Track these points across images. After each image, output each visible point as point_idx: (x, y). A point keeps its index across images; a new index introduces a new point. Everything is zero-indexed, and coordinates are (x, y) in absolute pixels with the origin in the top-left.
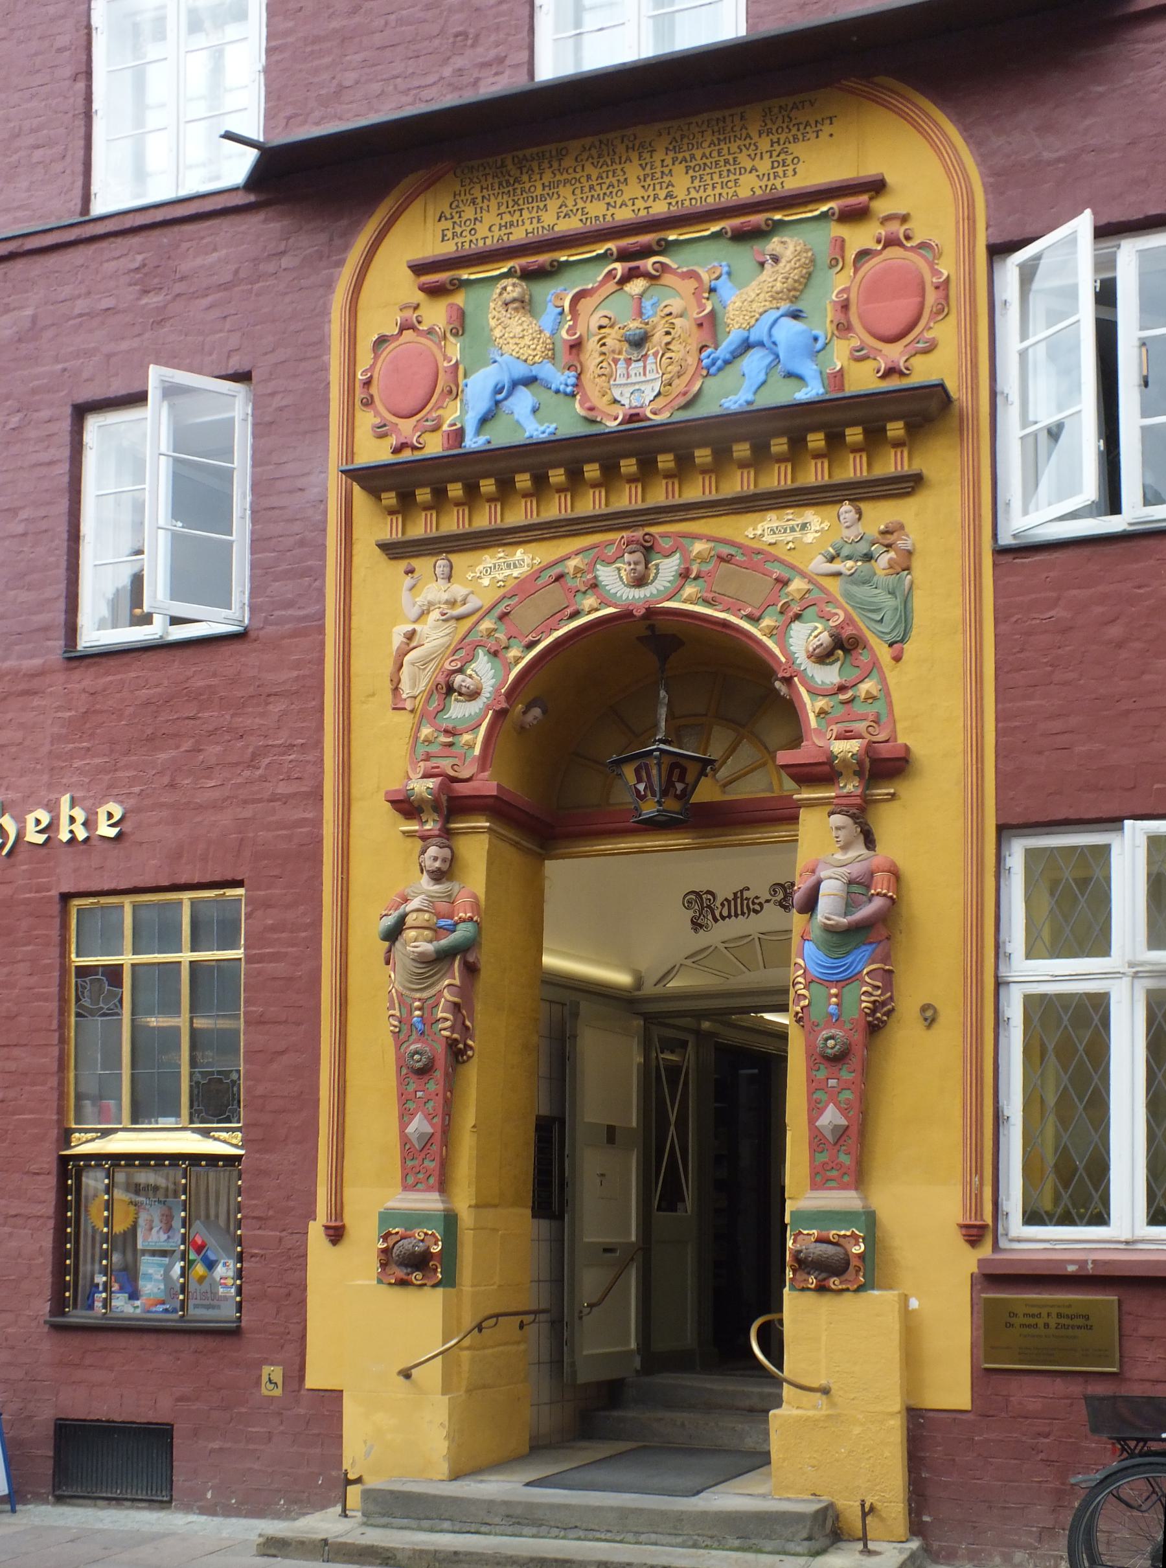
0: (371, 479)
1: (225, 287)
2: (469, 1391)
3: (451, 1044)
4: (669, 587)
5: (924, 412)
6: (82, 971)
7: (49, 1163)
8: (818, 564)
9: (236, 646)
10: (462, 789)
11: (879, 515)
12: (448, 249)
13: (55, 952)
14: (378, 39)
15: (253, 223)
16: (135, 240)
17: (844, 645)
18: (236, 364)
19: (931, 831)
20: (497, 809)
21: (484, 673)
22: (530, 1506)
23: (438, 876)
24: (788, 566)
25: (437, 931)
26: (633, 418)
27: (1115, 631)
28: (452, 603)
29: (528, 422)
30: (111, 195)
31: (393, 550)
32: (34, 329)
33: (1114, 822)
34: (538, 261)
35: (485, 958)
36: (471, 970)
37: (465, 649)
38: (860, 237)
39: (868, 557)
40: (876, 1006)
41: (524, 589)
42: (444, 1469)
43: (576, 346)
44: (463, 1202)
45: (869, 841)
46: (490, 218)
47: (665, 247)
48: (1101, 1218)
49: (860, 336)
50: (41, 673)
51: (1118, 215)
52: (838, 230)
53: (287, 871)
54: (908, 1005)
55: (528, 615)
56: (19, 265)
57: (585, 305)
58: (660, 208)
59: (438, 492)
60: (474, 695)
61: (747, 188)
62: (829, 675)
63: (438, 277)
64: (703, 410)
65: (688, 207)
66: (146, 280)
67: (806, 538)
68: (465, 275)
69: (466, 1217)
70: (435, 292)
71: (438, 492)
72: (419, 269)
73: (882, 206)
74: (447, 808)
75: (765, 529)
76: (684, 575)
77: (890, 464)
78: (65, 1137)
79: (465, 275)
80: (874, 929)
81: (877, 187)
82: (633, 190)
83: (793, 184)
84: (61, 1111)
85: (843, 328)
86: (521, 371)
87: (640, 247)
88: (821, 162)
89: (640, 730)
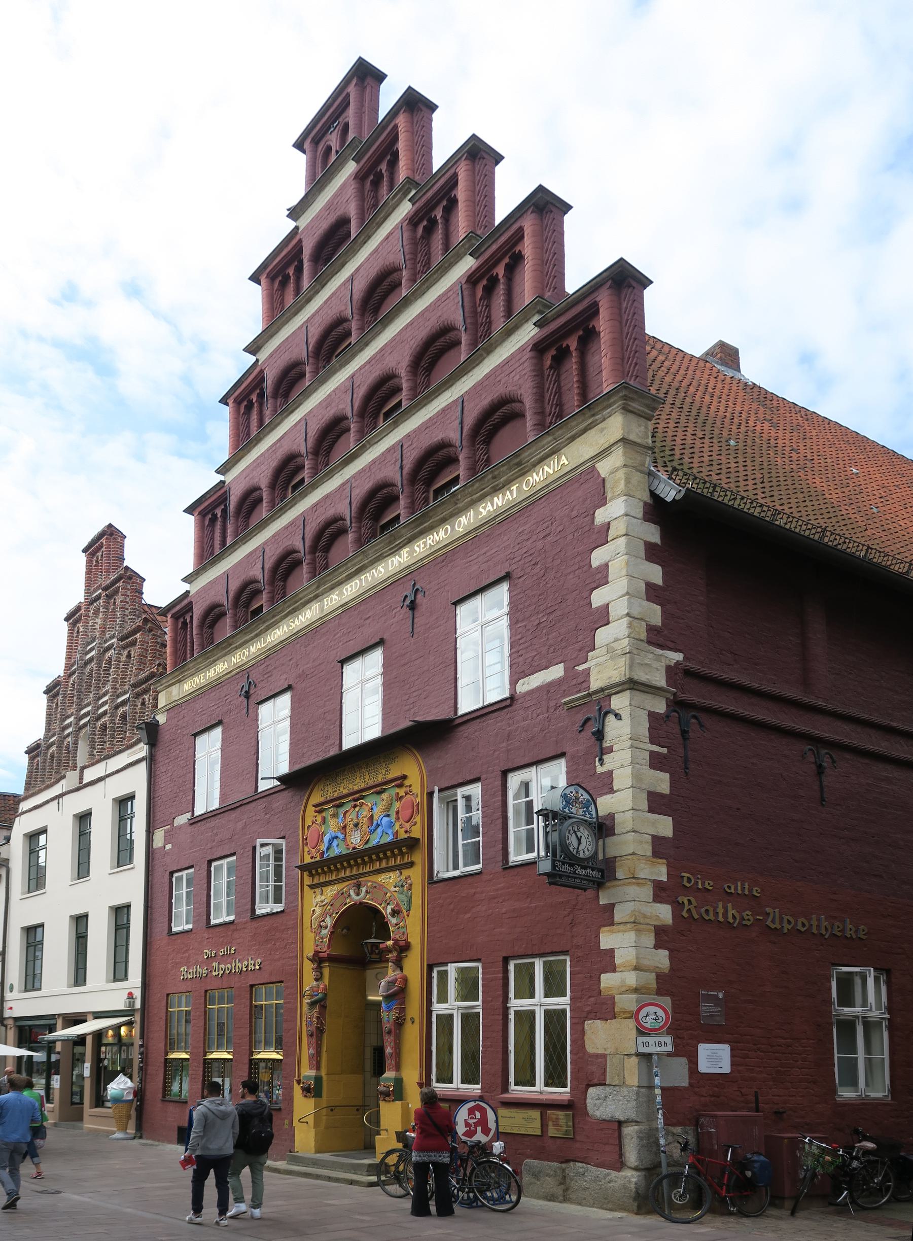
0: (303, 868)
1: (280, 812)
2: (326, 1128)
3: (317, 1028)
4: (363, 897)
5: (412, 844)
6: (256, 1006)
7: (247, 1061)
8: (393, 889)
9: (282, 915)
10: (321, 955)
11: (406, 873)
12: (322, 800)
13: (248, 1001)
14: (311, 739)
15: (285, 793)
16: (264, 800)
17: (395, 913)
18: (282, 834)
19: (413, 966)
20: (331, 959)
21: (329, 922)
22: (317, 1160)
23: (316, 980)
24: (387, 887)
25: (312, 996)
26: (354, 848)
27: (452, 907)
28: (322, 902)
29: (336, 851)
30: (350, 741)
31: (312, 887)
32: (246, 825)
33: (446, 964)
34: (338, 803)
35: (329, 1002)
36: (324, 1007)
37: (324, 915)
38: (401, 792)
39: (402, 886)
40: (398, 1019)
41: (335, 897)
42: (313, 1150)
43: (345, 827)
44: (323, 1073)
45: (402, 970)
46: (330, 790)
47: (363, 797)
48: (451, 1082)
49: (402, 821)
50: (246, 923)
51: (443, 786)
52: (397, 790)
53: (286, 979)
54: (408, 1018)
55: (337, 904)
56: (243, 807)
57: (348, 814)
58: (363, 786)
59: (321, 870)
60: (326, 927)
61: (380, 779)
62: (394, 921)
63: (320, 808)
64: (370, 845)
65: (369, 785)
66: (266, 810)
67: (390, 879)
68: (324, 807)
69: (325, 1078)
70: (319, 812)
71: (321, 870)
72: (315, 806)
73: (407, 783)
74: (318, 960)
75: (382, 878)
76: (367, 892)
77: (407, 859)
78: (251, 1054)
79: (324, 807)
80: (399, 994)
81: (405, 777)
82: (358, 780)
83: (390, 776)
84: (204, 1047)
85: (398, 819)
86: (333, 835)
87: (358, 796)
88: (395, 771)
89: (362, 937)
